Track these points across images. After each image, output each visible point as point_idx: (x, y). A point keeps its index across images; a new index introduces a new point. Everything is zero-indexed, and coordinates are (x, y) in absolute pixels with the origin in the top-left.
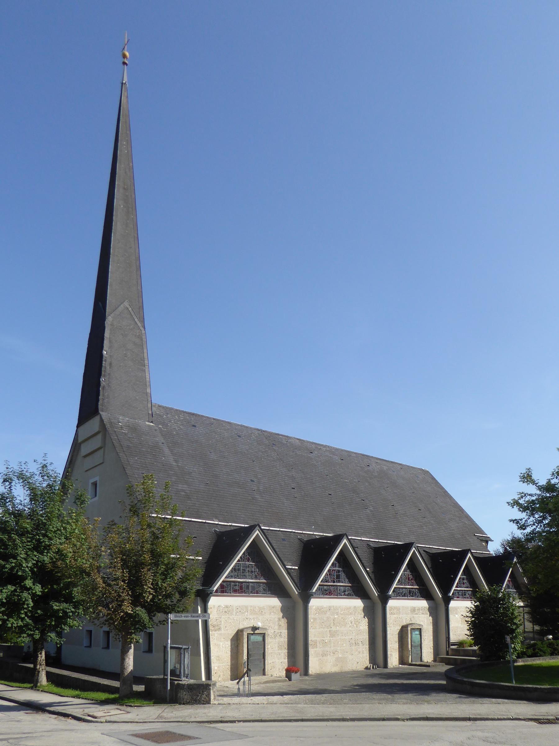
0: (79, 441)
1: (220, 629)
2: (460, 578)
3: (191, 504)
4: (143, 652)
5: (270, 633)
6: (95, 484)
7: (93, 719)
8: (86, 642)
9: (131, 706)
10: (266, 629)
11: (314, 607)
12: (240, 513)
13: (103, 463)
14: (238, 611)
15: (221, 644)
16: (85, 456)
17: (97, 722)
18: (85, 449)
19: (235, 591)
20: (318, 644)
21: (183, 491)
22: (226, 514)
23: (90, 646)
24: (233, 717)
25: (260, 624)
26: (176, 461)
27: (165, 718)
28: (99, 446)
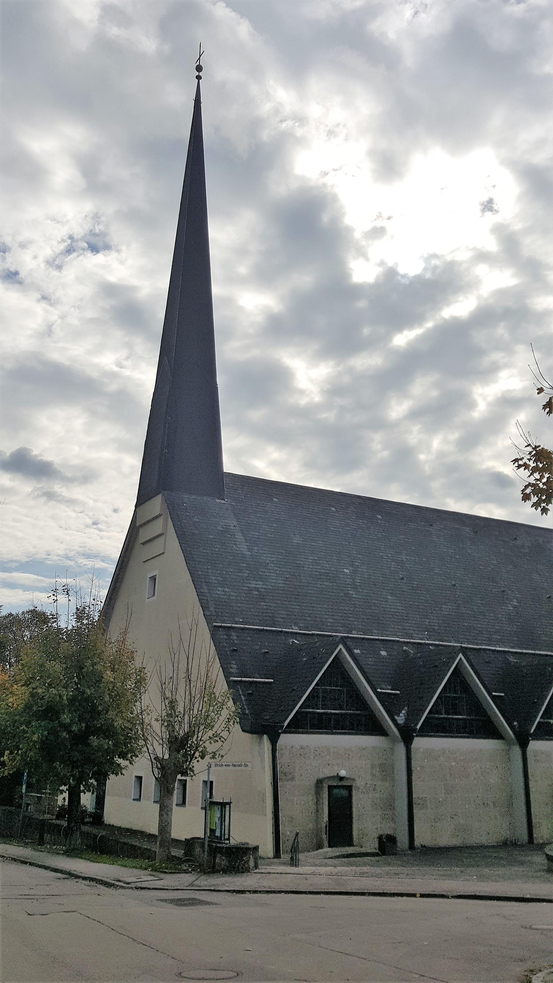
0: (138, 524)
1: (292, 779)
2: (539, 723)
3: (265, 607)
4: (134, 800)
5: (359, 783)
6: (153, 579)
7: (126, 885)
8: (133, 793)
9: (165, 873)
10: (353, 780)
11: (421, 750)
12: (327, 617)
13: (163, 553)
14: (317, 753)
15: (295, 799)
16: (143, 544)
17: (128, 888)
18: (144, 535)
19: (313, 726)
20: (428, 804)
21: (257, 589)
22: (308, 619)
23: (139, 799)
24: (270, 887)
25: (343, 773)
26: (249, 550)
27: (200, 886)
28: (160, 532)
